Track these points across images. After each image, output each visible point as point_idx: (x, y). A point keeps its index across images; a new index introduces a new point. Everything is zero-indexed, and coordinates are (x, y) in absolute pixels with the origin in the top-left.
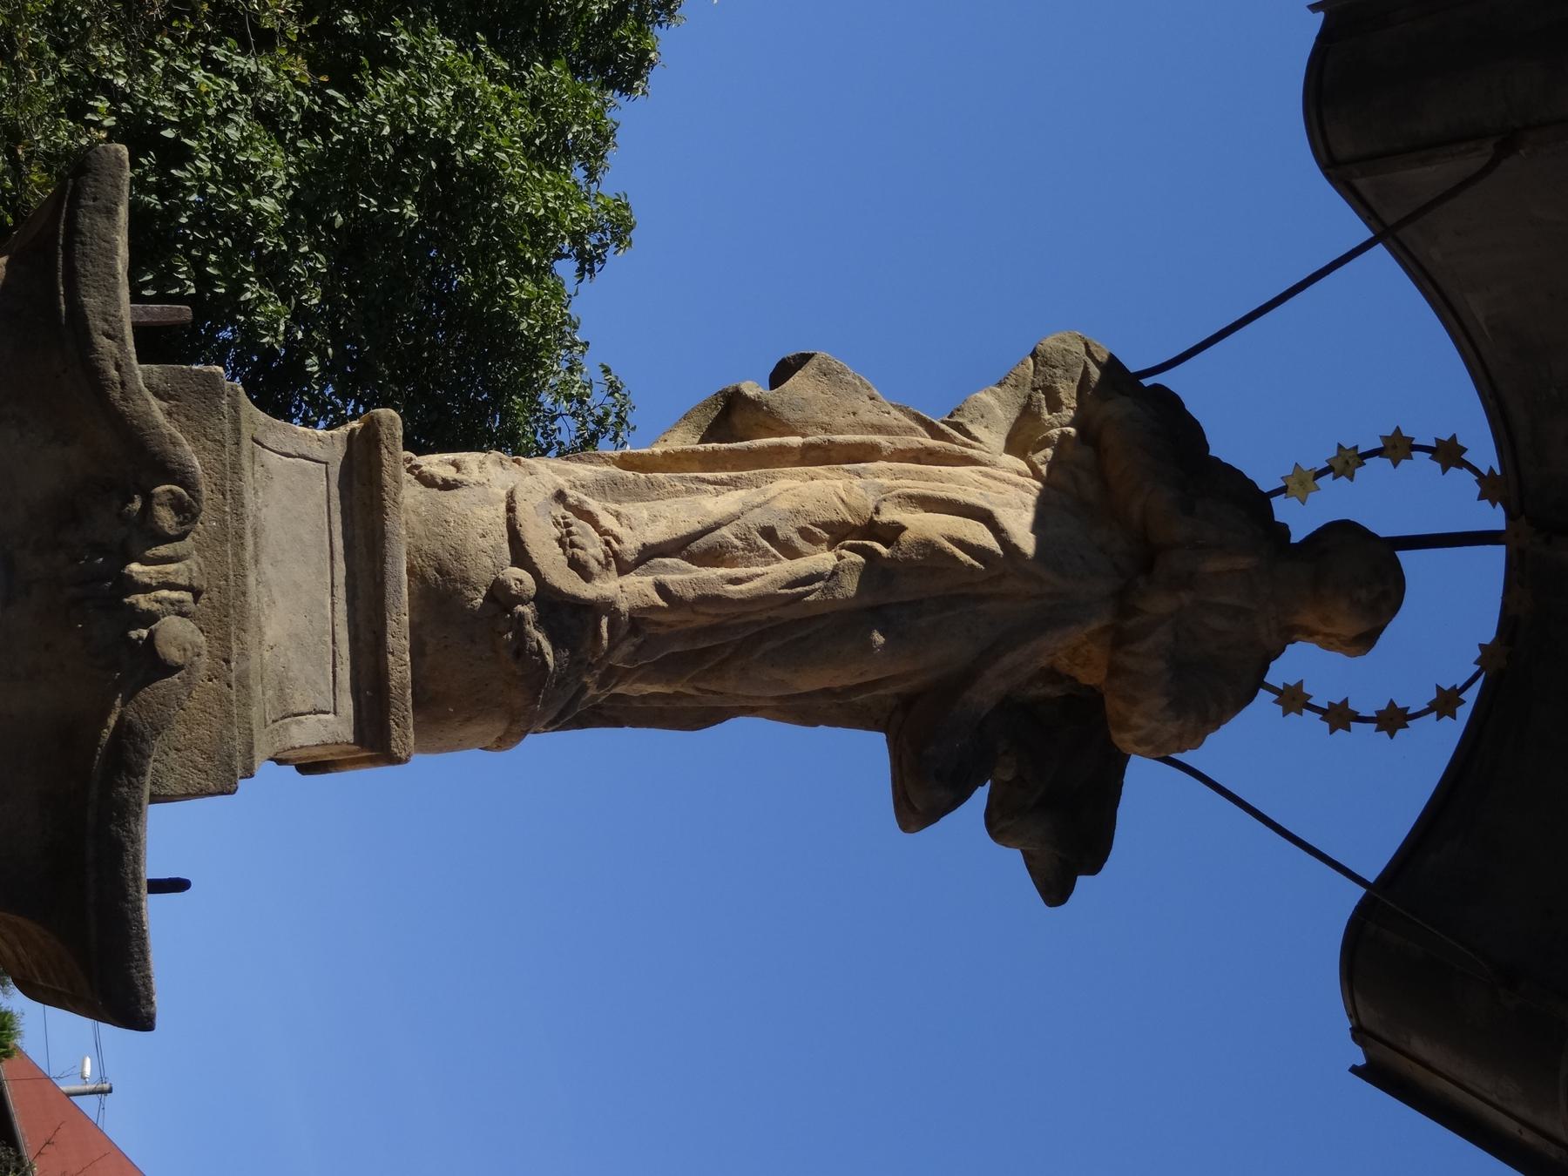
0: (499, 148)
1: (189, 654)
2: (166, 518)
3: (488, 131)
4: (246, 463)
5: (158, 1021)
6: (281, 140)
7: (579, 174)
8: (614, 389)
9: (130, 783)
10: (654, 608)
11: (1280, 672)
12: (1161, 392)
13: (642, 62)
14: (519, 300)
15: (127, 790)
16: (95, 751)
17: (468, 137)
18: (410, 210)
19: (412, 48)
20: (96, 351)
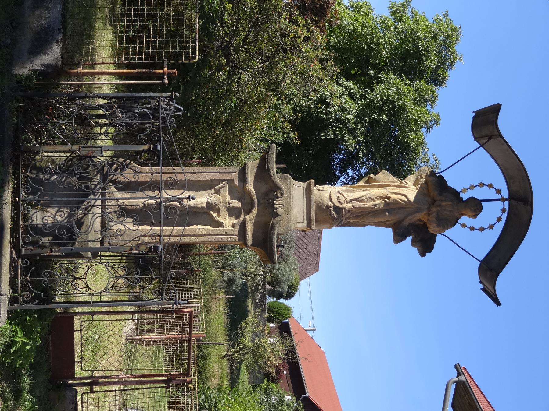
0: (406, 102)
2: (279, 195)
4: (291, 187)
6: (354, 101)
7: (428, 107)
8: (436, 160)
10: (352, 209)
11: (460, 221)
12: (441, 176)
13: (444, 79)
14: (411, 139)
17: (399, 99)
18: (385, 117)
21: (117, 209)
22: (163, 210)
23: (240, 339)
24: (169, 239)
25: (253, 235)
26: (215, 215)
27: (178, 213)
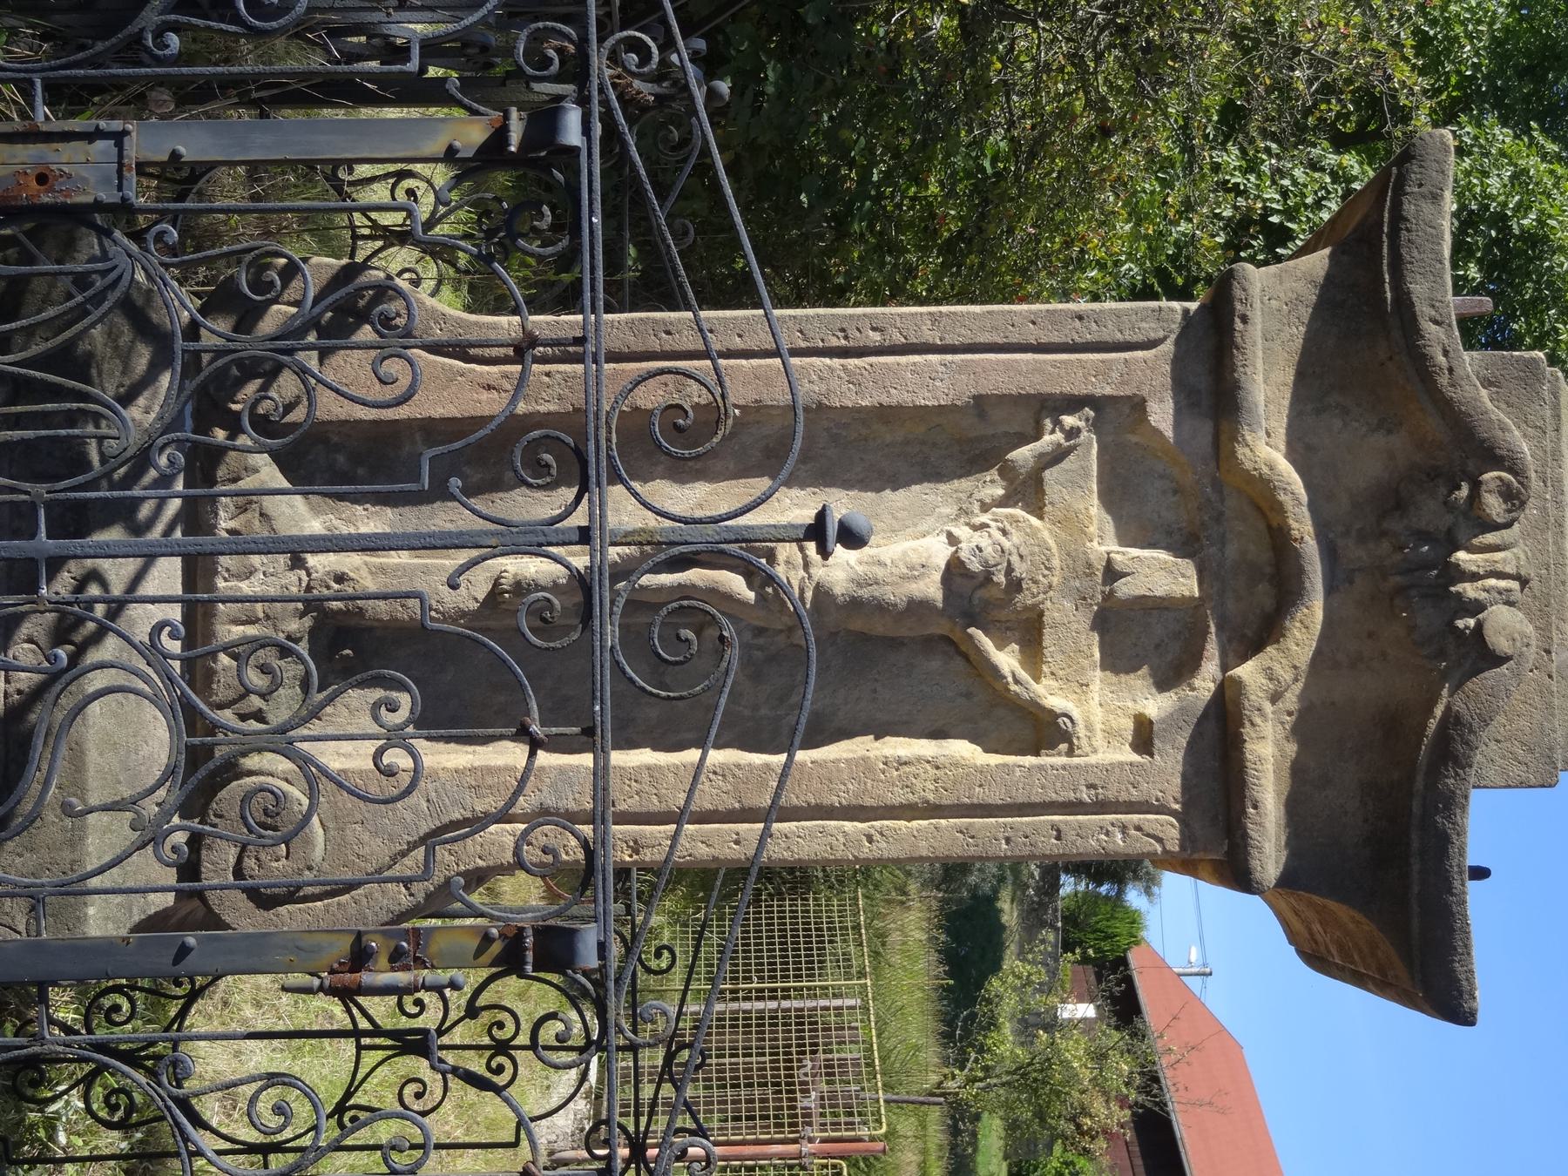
0: (1550, 216)
1: (1518, 644)
2: (1494, 505)
3: (1541, 203)
5: (1480, 1016)
9: (1457, 774)
15: (1453, 781)
16: (1420, 742)
19: (1476, 138)
20: (1423, 337)
21: (294, 626)
22: (611, 634)
23: (985, 1037)
24: (675, 838)
25: (1294, 806)
26: (1007, 660)
27: (733, 654)
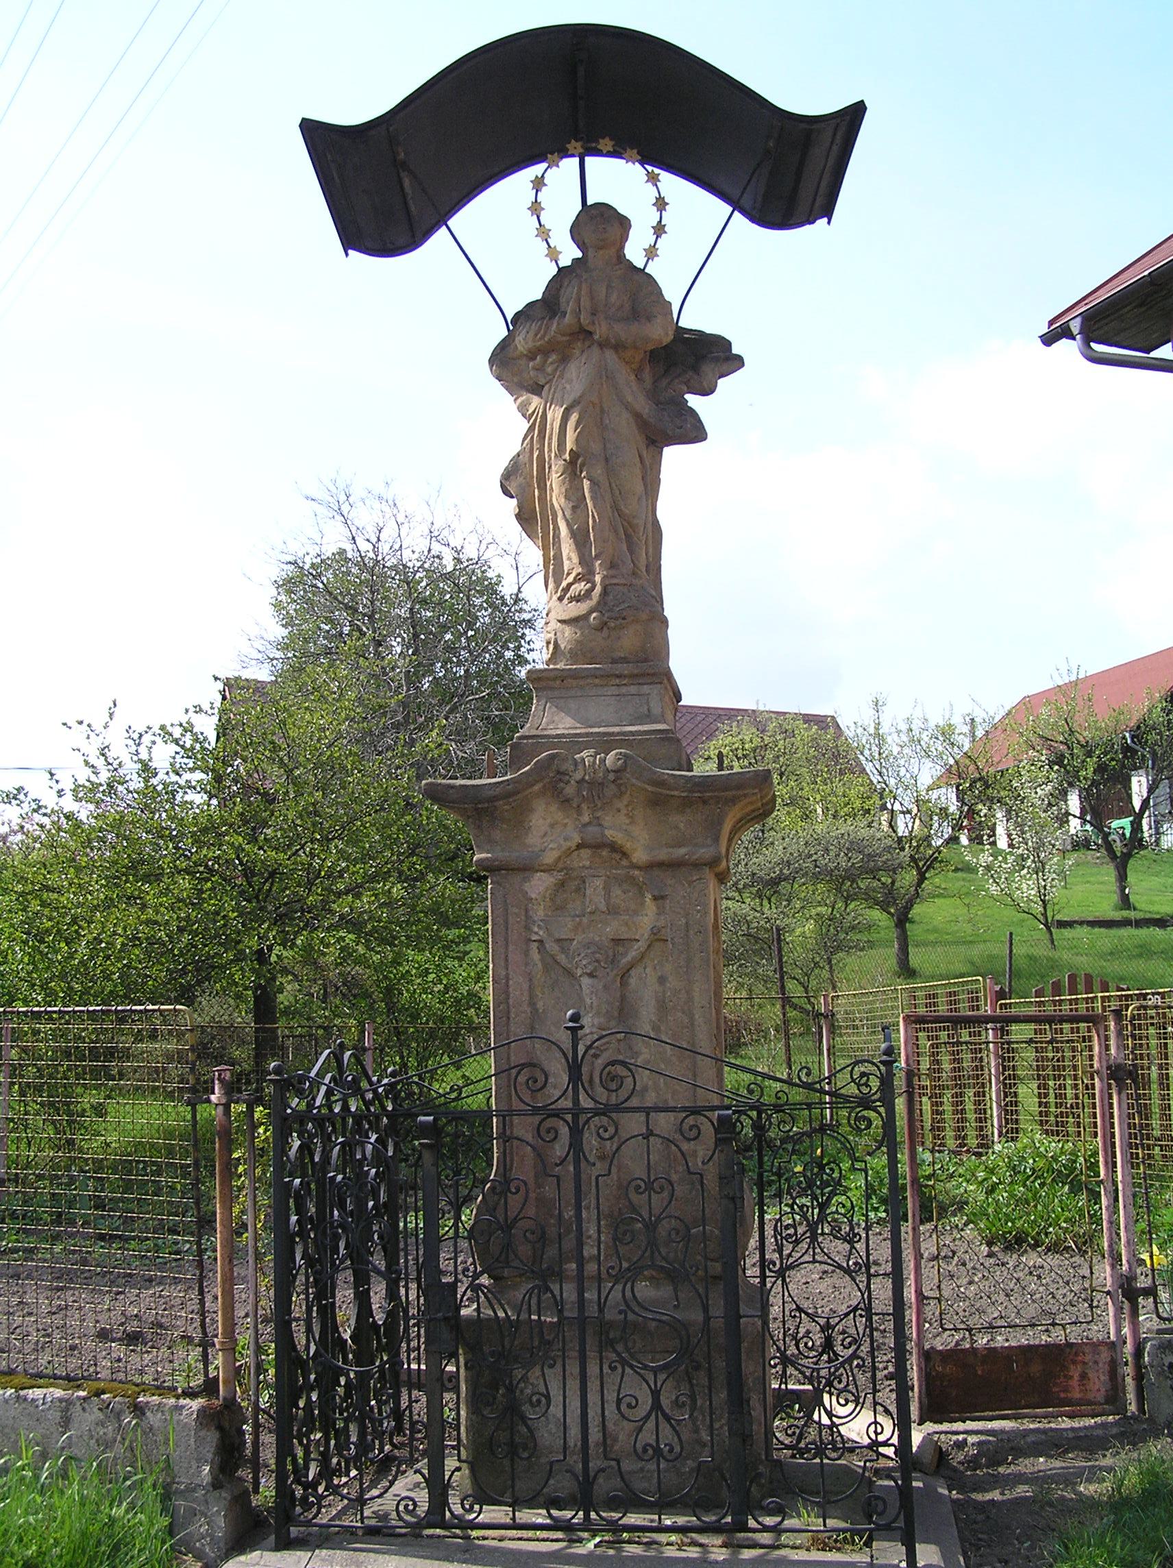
11: (639, 262)
